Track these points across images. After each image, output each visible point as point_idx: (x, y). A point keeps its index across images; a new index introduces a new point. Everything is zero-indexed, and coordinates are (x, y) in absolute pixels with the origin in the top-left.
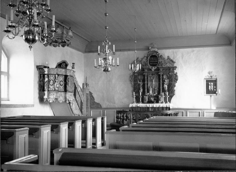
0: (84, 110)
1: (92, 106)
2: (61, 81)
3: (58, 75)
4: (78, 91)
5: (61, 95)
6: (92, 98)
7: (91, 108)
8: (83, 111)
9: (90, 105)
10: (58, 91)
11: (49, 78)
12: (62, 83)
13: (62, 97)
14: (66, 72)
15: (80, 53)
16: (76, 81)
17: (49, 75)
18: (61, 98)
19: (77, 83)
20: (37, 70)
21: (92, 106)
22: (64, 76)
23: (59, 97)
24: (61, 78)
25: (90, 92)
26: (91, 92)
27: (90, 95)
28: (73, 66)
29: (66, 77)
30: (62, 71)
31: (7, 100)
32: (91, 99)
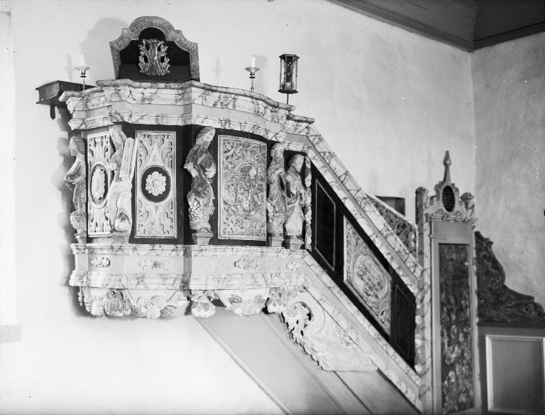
0: (428, 336)
1: (493, 313)
2: (150, 171)
3: (130, 130)
4: (369, 231)
5: (155, 265)
6: (491, 267)
7: (487, 322)
8: (418, 342)
9: (480, 306)
10: (133, 239)
11: (89, 154)
12: (157, 184)
13: (164, 277)
14: (188, 108)
15: (446, 50)
16: (340, 172)
17: (89, 137)
18: (153, 281)
19: (349, 185)
20: (53, 116)
21: (493, 313)
22: (173, 135)
23: (141, 279)
24: (161, 151)
25: (478, 234)
26: (484, 235)
27: (478, 250)
28: (289, 78)
29: (187, 135)
30: (159, 102)
31: (96, 289)
32: (487, 273)
